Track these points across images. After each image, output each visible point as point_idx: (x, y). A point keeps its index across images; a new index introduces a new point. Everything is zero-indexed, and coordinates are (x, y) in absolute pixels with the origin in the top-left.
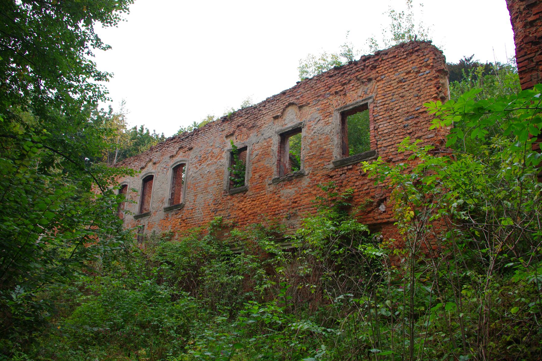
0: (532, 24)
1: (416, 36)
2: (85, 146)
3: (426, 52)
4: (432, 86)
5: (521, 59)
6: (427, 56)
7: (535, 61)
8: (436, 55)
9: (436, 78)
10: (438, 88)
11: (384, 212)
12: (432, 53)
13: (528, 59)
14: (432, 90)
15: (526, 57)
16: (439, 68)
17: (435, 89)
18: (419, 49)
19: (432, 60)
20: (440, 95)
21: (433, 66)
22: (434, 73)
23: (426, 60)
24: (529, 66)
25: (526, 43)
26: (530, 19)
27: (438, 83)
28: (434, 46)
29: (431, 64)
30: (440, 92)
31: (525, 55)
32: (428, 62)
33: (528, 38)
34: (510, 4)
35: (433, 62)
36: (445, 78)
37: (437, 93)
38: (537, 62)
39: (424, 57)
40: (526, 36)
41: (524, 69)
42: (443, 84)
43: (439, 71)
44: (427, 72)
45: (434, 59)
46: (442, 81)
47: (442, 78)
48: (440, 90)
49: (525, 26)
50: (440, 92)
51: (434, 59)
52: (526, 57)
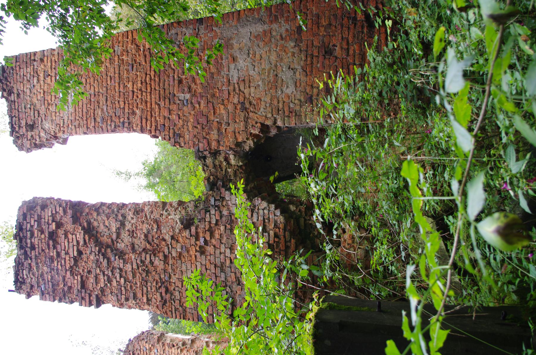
0: (148, 300)
1: (120, 350)
2: (389, 339)
3: (137, 346)
4: (170, 351)
5: (174, 315)
6: (142, 347)
7: (178, 307)
8: (143, 339)
9: (164, 345)
10: (174, 346)
11: (398, 170)
12: (140, 342)
13: (175, 310)
14: (173, 351)
15: (173, 312)
16: (156, 340)
17: (173, 349)
18: (133, 352)
19: (147, 344)
20: (181, 345)
21: (152, 345)
22: (159, 346)
23: (145, 350)
24: (181, 312)
25: (163, 308)
26: (145, 300)
27: (168, 345)
28: (135, 337)
29: (150, 346)
30: (177, 345)
31: (172, 312)
32: (148, 348)
33: (159, 307)
34: (127, 307)
35: (149, 345)
36: (167, 337)
37: (178, 348)
38: (180, 306)
39: (142, 350)
40: (157, 307)
41: (182, 316)
42: (171, 340)
43: (159, 341)
44: (156, 351)
45: (146, 342)
46: (168, 341)
47: (165, 340)
48: (175, 345)
49: (149, 304)
50: (177, 345)
51: (146, 342)
52: (173, 312)
